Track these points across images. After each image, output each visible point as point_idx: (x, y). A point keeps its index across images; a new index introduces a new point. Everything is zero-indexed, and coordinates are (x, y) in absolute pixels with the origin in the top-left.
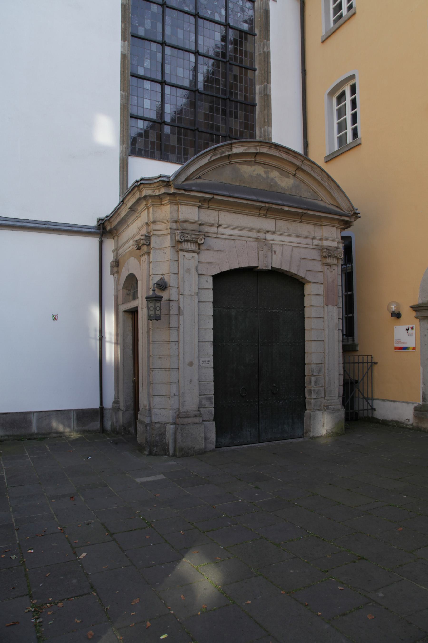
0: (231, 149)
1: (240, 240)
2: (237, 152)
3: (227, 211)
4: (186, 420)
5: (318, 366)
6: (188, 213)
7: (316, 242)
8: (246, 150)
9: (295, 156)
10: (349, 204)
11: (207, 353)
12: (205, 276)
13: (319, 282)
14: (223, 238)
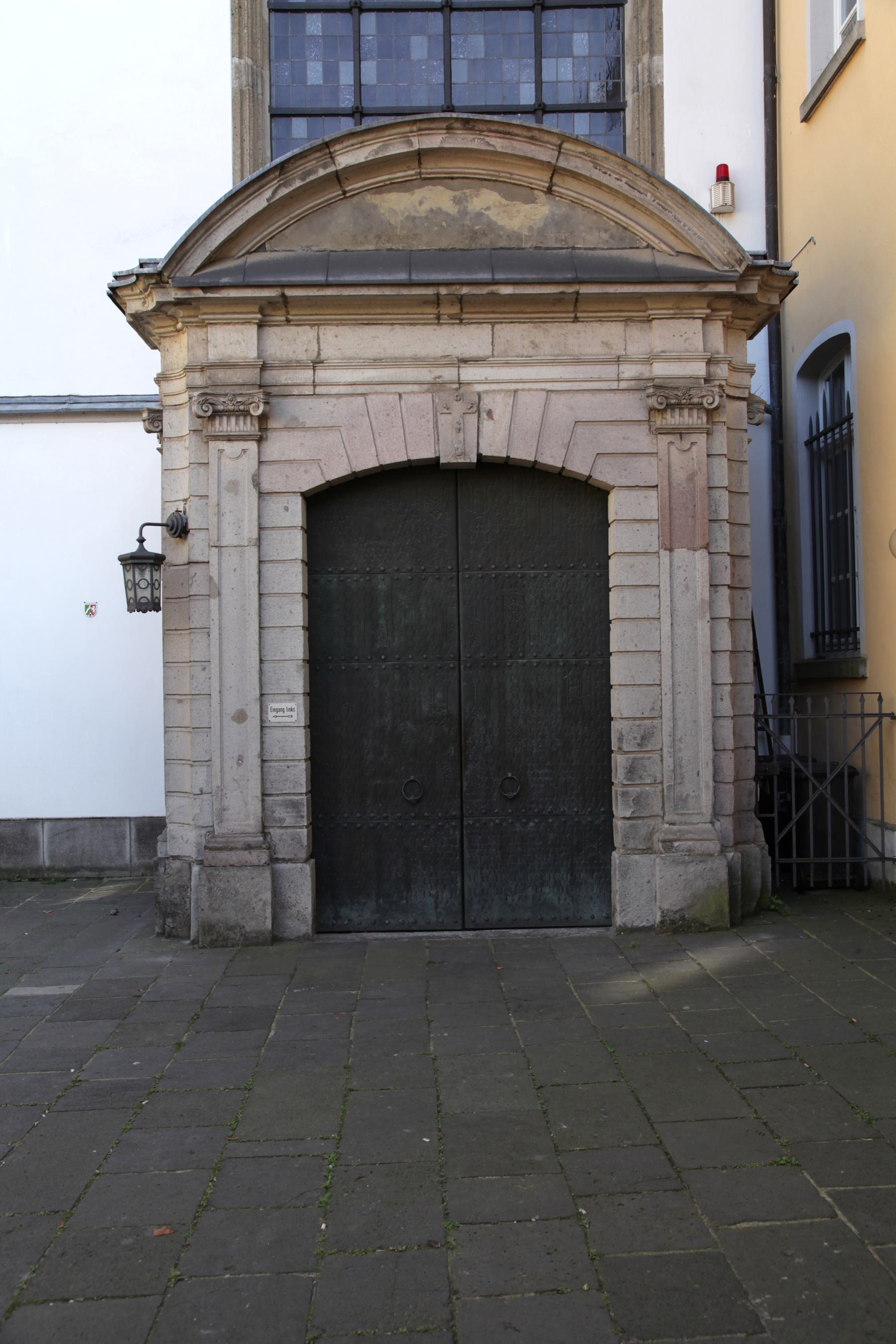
0: (332, 158)
1: (382, 393)
2: (351, 164)
3: (342, 323)
4: (224, 856)
5: (639, 726)
6: (231, 344)
7: (630, 371)
8: (377, 152)
9: (532, 138)
10: (728, 244)
11: (289, 690)
12: (282, 495)
13: (642, 485)
14: (332, 393)
